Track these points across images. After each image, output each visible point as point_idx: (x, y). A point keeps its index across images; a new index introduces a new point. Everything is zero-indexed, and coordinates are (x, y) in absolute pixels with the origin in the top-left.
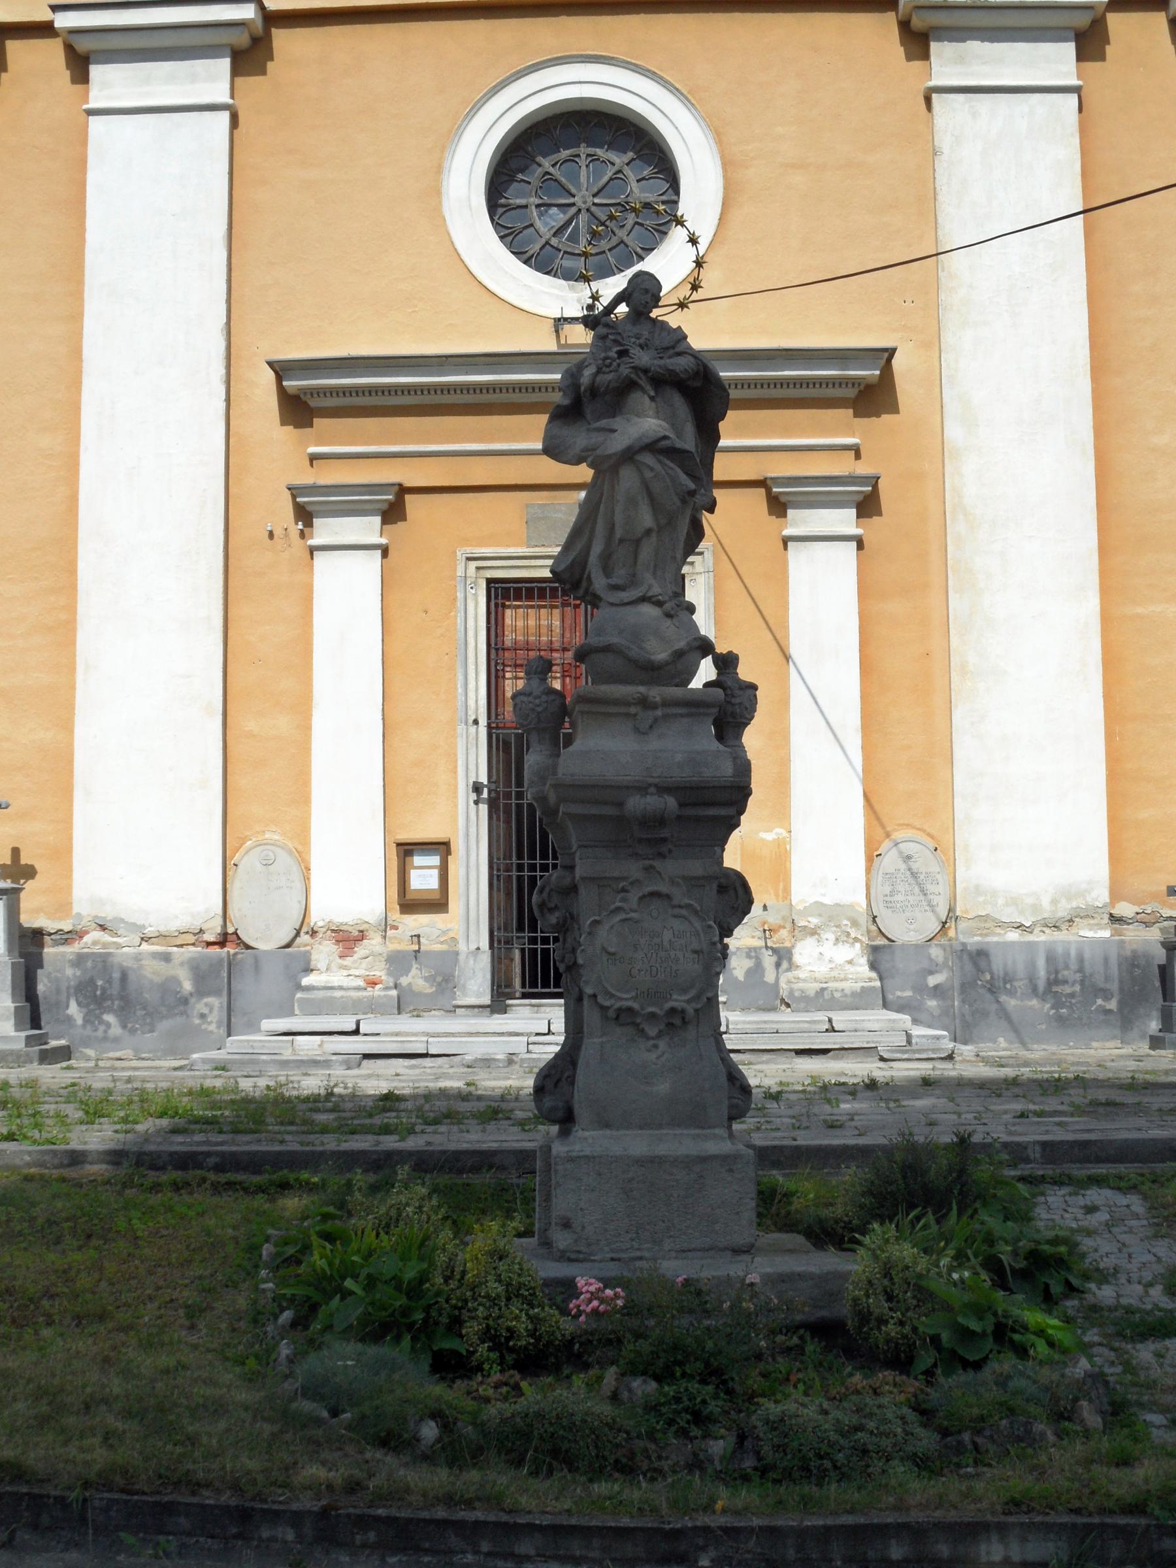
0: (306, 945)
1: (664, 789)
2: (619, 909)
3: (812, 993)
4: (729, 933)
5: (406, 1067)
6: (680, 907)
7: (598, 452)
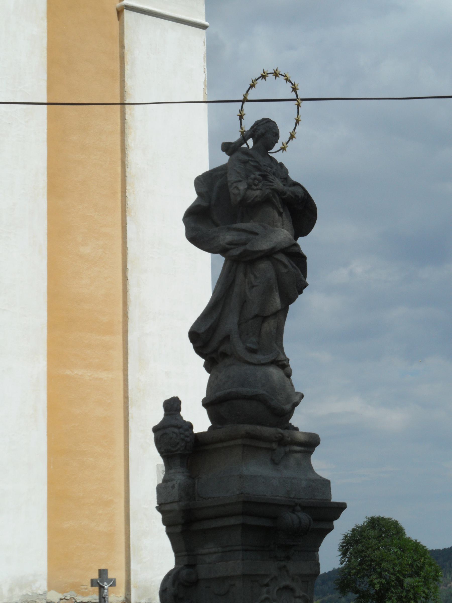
7: (248, 247)
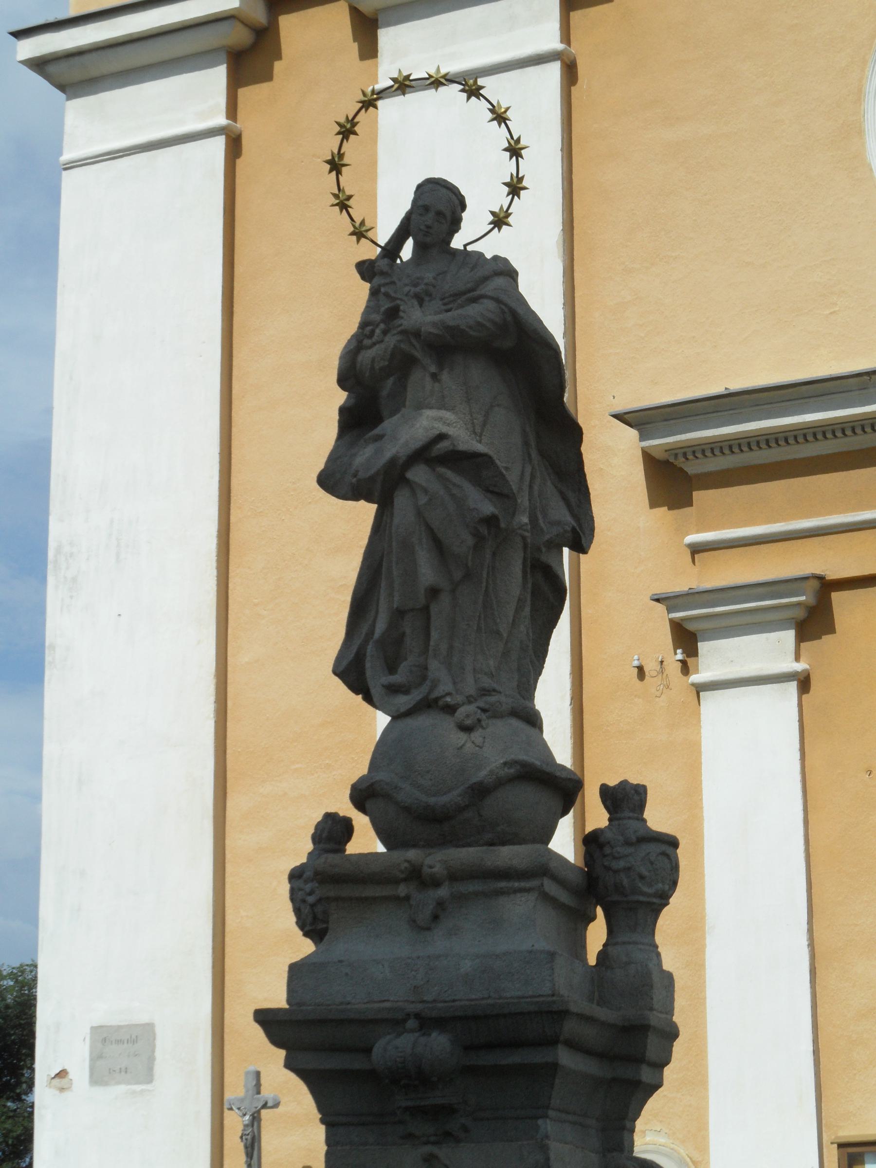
1: (427, 1023)
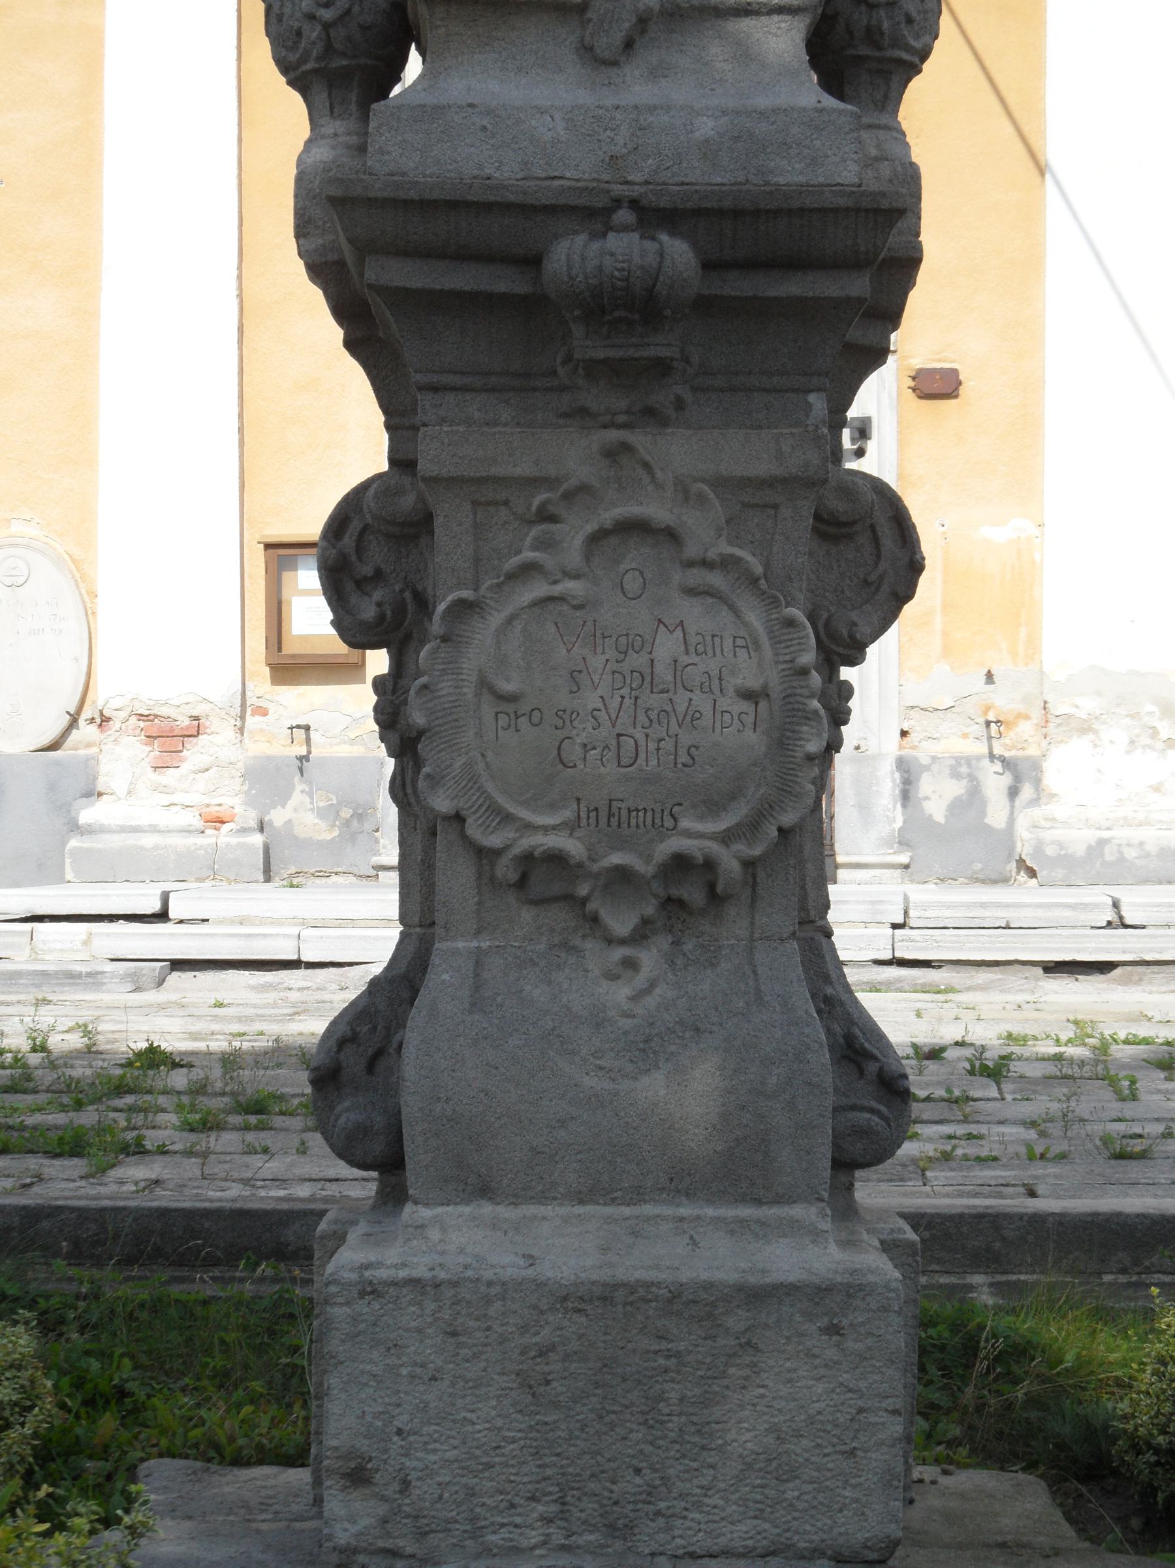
0: (89, 745)
1: (655, 216)
2: (528, 570)
3: (1080, 850)
4: (855, 656)
5: (254, 988)
6: (706, 564)
